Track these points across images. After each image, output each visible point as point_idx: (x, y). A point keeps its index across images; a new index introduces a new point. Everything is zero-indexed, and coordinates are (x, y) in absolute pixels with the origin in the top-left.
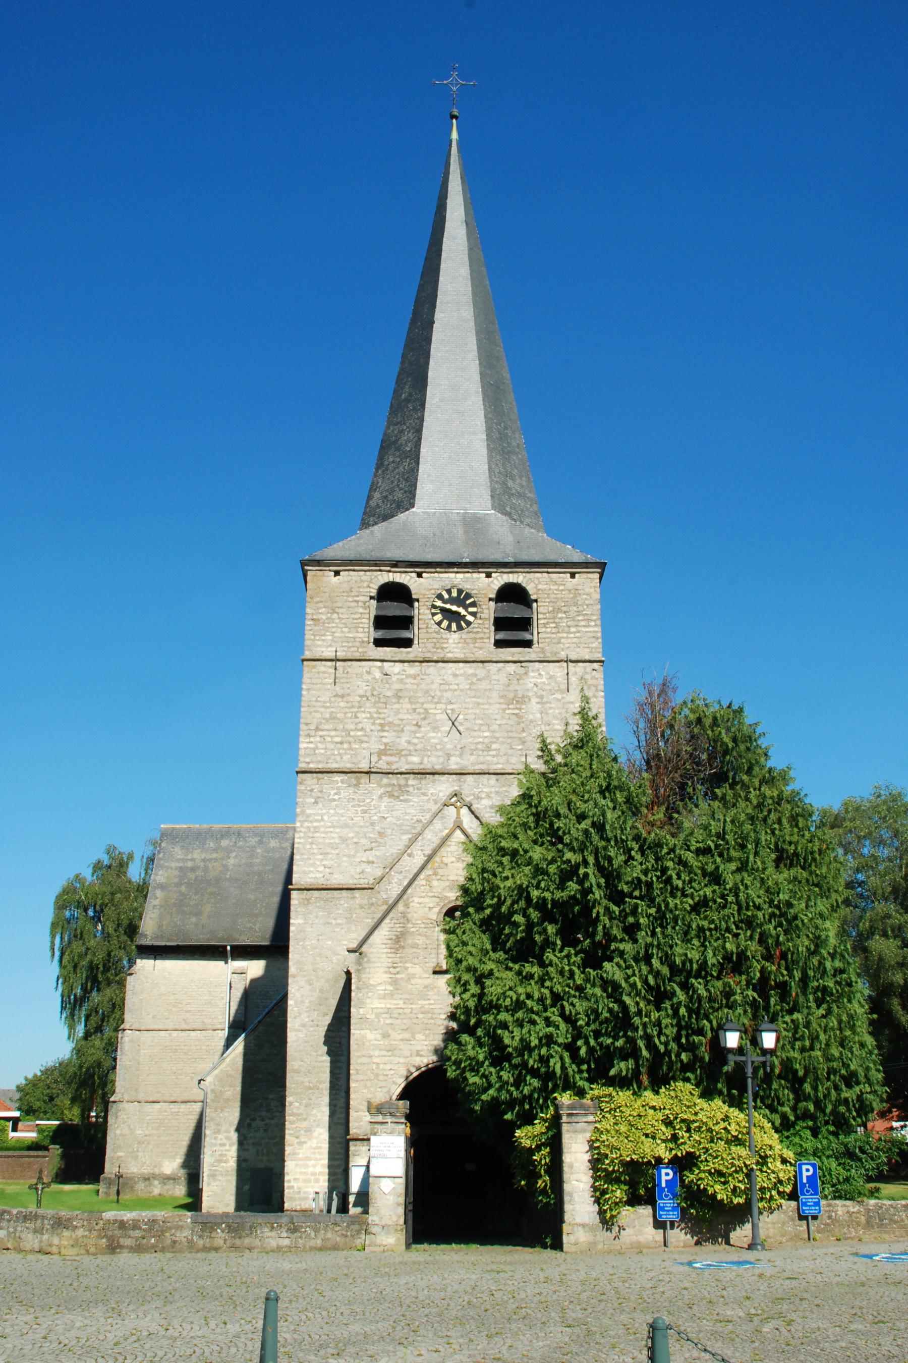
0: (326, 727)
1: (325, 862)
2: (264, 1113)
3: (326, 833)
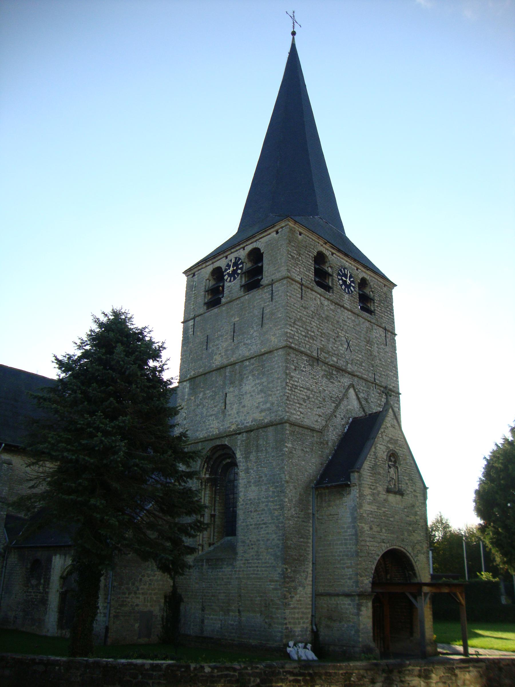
0: (298, 324)
1: (301, 410)
2: (149, 572)
3: (301, 391)
